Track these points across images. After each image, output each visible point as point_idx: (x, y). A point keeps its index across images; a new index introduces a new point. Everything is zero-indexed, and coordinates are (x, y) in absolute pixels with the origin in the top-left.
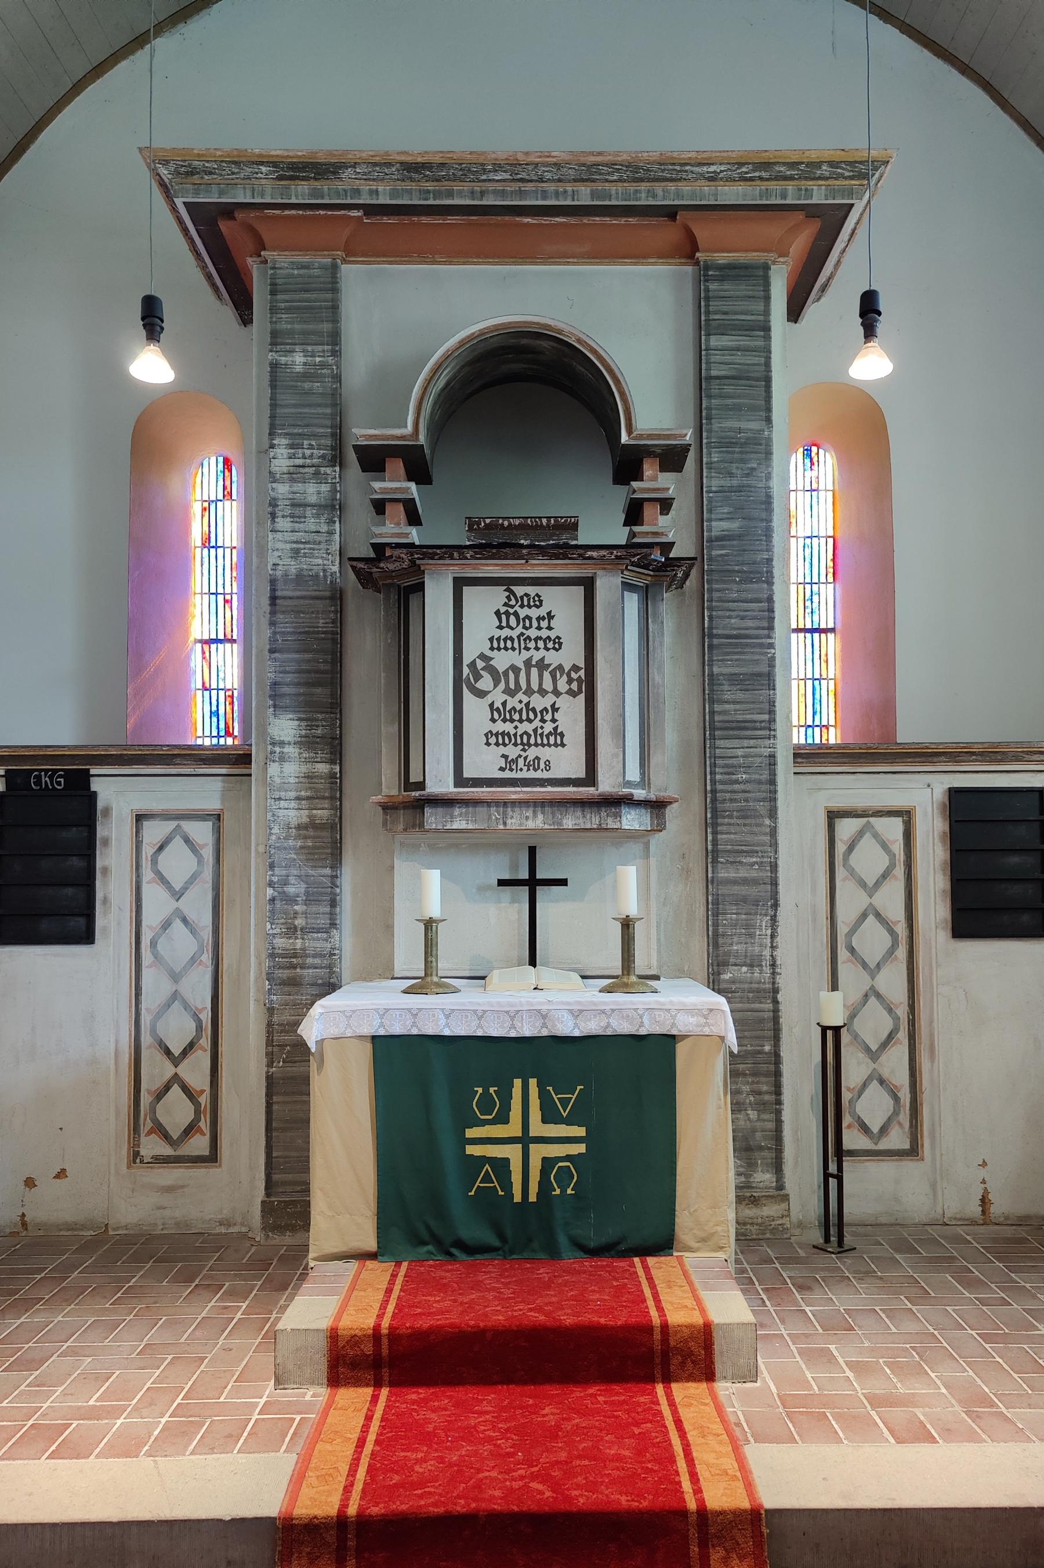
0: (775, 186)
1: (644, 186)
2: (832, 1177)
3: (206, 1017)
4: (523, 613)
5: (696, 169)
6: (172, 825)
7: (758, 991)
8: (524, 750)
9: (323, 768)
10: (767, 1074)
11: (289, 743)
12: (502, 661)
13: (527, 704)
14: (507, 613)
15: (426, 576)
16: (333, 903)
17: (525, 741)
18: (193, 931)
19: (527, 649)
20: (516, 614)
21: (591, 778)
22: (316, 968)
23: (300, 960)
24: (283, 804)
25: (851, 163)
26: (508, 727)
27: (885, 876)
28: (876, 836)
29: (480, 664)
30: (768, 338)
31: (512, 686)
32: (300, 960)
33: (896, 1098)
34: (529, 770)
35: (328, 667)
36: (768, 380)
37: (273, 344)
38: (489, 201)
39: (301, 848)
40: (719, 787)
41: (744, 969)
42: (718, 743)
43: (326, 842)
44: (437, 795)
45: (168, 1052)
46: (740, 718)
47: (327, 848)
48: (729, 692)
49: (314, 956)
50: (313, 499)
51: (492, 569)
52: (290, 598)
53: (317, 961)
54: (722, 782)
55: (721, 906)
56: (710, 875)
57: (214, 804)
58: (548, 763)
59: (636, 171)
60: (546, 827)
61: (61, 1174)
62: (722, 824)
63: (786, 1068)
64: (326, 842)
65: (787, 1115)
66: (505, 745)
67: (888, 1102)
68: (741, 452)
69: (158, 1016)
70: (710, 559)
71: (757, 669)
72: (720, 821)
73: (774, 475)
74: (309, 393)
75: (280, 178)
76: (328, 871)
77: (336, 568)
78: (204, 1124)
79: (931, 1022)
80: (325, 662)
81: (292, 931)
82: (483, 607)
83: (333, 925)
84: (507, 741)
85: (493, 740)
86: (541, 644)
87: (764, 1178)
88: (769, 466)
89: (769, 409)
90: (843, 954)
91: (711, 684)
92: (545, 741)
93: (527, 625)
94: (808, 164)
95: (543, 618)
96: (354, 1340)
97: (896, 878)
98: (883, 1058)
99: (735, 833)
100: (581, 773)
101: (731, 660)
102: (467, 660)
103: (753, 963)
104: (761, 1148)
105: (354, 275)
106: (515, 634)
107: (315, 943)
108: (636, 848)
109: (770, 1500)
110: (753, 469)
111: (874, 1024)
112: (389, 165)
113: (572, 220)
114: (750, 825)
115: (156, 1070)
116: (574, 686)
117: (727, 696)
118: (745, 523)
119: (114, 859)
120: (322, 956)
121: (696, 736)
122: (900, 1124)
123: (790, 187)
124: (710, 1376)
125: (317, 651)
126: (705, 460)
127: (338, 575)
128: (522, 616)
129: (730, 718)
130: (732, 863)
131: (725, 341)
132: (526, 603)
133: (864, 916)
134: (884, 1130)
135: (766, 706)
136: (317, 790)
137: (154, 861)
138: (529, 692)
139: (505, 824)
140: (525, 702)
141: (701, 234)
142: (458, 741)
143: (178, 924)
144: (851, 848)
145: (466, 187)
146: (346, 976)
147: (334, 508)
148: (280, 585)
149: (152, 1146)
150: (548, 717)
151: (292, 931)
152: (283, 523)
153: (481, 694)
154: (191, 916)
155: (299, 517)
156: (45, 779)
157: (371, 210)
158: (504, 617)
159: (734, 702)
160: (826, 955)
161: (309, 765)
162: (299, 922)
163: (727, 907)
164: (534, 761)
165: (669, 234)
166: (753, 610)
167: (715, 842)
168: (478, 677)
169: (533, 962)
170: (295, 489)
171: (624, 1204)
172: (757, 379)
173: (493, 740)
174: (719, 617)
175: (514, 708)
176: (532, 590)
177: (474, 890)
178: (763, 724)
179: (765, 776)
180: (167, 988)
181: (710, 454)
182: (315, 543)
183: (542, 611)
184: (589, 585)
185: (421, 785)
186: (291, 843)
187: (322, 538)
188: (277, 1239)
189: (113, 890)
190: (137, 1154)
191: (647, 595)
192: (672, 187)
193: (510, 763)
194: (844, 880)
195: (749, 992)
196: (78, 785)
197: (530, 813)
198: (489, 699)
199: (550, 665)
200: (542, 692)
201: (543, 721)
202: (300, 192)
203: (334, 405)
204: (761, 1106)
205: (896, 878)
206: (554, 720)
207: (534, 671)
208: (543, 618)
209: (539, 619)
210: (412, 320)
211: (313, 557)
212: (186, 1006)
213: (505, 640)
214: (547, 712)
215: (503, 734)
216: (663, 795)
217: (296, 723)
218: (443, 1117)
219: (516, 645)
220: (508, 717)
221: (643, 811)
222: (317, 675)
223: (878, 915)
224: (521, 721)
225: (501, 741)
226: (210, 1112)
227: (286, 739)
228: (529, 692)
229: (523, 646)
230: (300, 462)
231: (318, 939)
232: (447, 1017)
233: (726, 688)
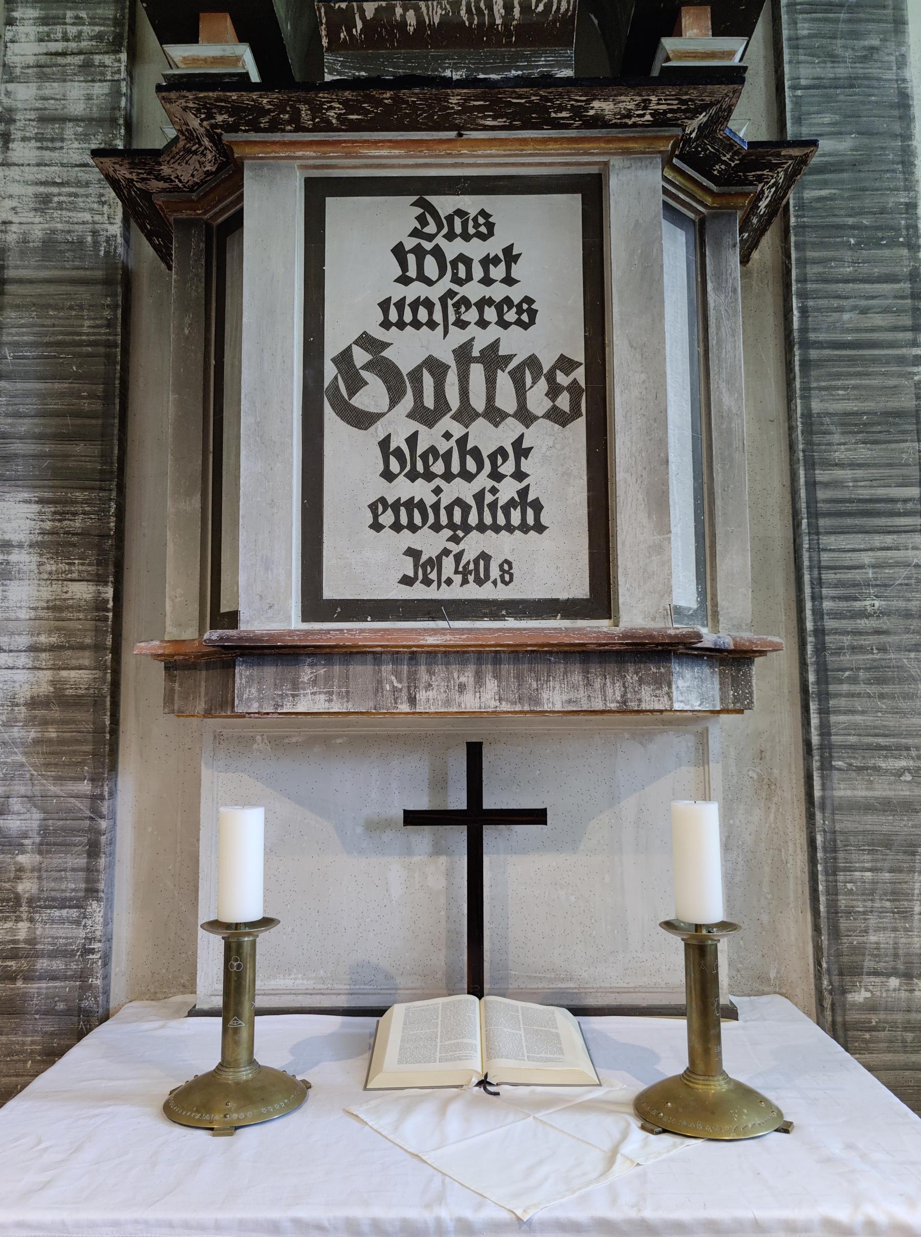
4: (451, 250)
8: (455, 539)
9: (82, 591)
11: (20, 546)
12: (407, 349)
13: (462, 441)
14: (419, 252)
15: (247, 174)
16: (93, 850)
17: (457, 518)
19: (462, 324)
20: (438, 253)
21: (601, 598)
22: (54, 978)
23: (24, 964)
26: (421, 490)
29: (361, 357)
31: (429, 402)
32: (24, 964)
34: (465, 582)
35: (98, 406)
39: (37, 742)
40: (830, 624)
41: (894, 982)
42: (825, 540)
44: (259, 638)
46: (865, 493)
47: (85, 742)
48: (842, 447)
49: (53, 955)
50: (77, 108)
51: (386, 155)
52: (31, 282)
53: (58, 965)
54: (837, 615)
55: (841, 855)
56: (817, 793)
58: (507, 568)
60: (505, 707)
62: (838, 695)
66: (413, 528)
68: (850, 21)
70: (801, 206)
71: (894, 404)
72: (832, 688)
76: (85, 787)
77: (116, 229)
80: (92, 396)
82: (367, 241)
83: (92, 892)
84: (418, 520)
85: (387, 518)
86: (490, 314)
88: (901, 43)
91: (809, 430)
92: (501, 521)
93: (462, 273)
95: (496, 261)
99: (863, 713)
100: (581, 589)
101: (845, 388)
102: (332, 348)
106: (434, 293)
107: (54, 929)
108: (680, 743)
110: (873, 49)
114: (892, 696)
116: (564, 402)
117: (840, 454)
118: (865, 140)
120: (66, 954)
125: (77, 377)
126: (785, 33)
127: (120, 240)
128: (450, 257)
129: (846, 494)
130: (860, 769)
132: (458, 229)
136: (69, 633)
138: (466, 415)
139: (412, 701)
140: (457, 435)
142: (301, 518)
146: (119, 988)
150: (507, 468)
153: (362, 420)
155: (52, 140)
158: (411, 259)
159: (853, 465)
161: (57, 587)
163: (854, 857)
164: (476, 562)
166: (885, 297)
168: (355, 384)
170: (48, 92)
173: (387, 518)
174: (818, 310)
175: (433, 450)
176: (471, 204)
177: (359, 830)
178: (909, 506)
181: (794, 23)
182: (78, 184)
183: (494, 247)
184: (592, 191)
185: (233, 619)
186: (17, 732)
191: (701, 235)
193: (425, 568)
195: (905, 1029)
198: (379, 430)
199: (510, 358)
200: (494, 415)
201: (496, 476)
206: (519, 475)
207: (477, 372)
208: (496, 261)
209: (486, 262)
211: (75, 209)
213: (415, 306)
214: (505, 457)
215: (410, 504)
216: (747, 637)
217: (36, 508)
219: (438, 316)
220: (420, 467)
221: (707, 671)
222: (79, 421)
224: (448, 476)
225: (404, 520)
227: (15, 538)
228: (466, 415)
229: (452, 318)
230: (59, 46)
231: (62, 921)
233: (836, 438)
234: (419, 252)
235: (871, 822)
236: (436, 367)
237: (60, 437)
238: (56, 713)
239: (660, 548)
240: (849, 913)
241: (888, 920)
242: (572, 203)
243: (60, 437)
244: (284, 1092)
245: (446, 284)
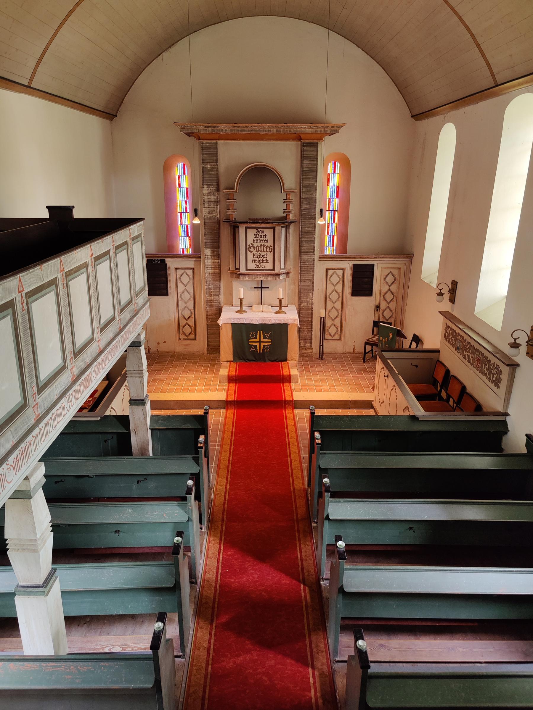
2: (321, 345)
3: (193, 311)
4: (260, 234)
9: (217, 261)
16: (219, 290)
21: (274, 269)
26: (257, 259)
28: (337, 274)
29: (251, 245)
33: (337, 329)
36: (317, 171)
43: (217, 276)
45: (185, 318)
50: (213, 200)
57: (192, 267)
61: (165, 342)
63: (313, 324)
64: (217, 276)
65: (313, 333)
69: (183, 311)
73: (317, 195)
78: (193, 333)
81: (211, 295)
82: (251, 233)
87: (308, 345)
89: (316, 179)
90: (328, 299)
96: (232, 376)
105: (220, 143)
107: (216, 298)
109: (295, 399)
111: (334, 314)
115: (183, 322)
121: (297, 253)
124: (290, 382)
133: (333, 291)
134: (334, 335)
137: (180, 278)
138: (261, 251)
142: (247, 261)
143: (186, 292)
144: (331, 277)
147: (217, 202)
149: (183, 337)
151: (211, 295)
152: (206, 206)
153: (251, 252)
154: (189, 290)
156: (156, 261)
160: (324, 300)
162: (212, 293)
167: (301, 277)
168: (250, 248)
169: (261, 304)
171: (277, 352)
179: (312, 263)
180: (184, 305)
183: (264, 234)
184: (274, 228)
185: (239, 269)
188: (210, 356)
189: (172, 284)
193: (257, 266)
196: (163, 261)
200: (264, 251)
203: (217, 177)
210: (235, 154)
212: (188, 309)
218: (245, 338)
223: (336, 291)
226: (194, 330)
228: (261, 251)
244: (245, 311)
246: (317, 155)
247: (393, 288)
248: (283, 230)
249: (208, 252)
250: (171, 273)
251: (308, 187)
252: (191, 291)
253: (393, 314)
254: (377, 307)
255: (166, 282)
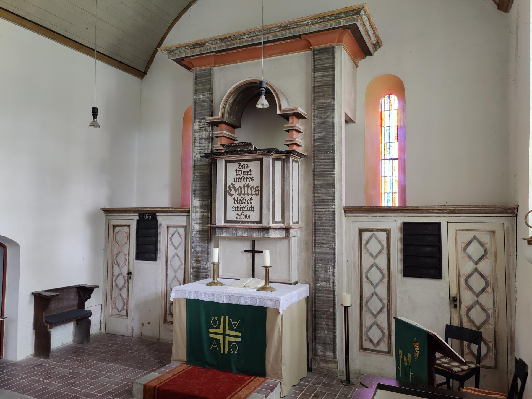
0: (329, 23)
1: (287, 31)
4: (243, 170)
5: (302, 23)
6: (175, 229)
7: (328, 291)
9: (206, 214)
10: (331, 319)
12: (237, 185)
16: (208, 254)
18: (180, 259)
20: (241, 171)
21: (261, 222)
24: (196, 225)
25: (351, 11)
26: (238, 205)
27: (380, 253)
28: (376, 238)
29: (231, 186)
30: (334, 71)
36: (334, 85)
37: (195, 93)
38: (244, 44)
41: (324, 283)
46: (323, 198)
50: (204, 137)
51: (233, 157)
53: (204, 270)
54: (318, 220)
59: (283, 28)
61: (149, 323)
67: (380, 333)
70: (314, 146)
71: (329, 182)
74: (203, 106)
75: (191, 49)
76: (206, 244)
79: (396, 307)
82: (233, 168)
83: (208, 260)
86: (248, 180)
87: (330, 354)
89: (334, 95)
90: (364, 279)
94: (336, 14)
97: (383, 253)
98: (378, 317)
103: (327, 281)
104: (329, 344)
106: (241, 177)
110: (329, 115)
111: (375, 305)
112: (216, 40)
113: (272, 44)
119: (162, 238)
120: (205, 269)
121: (311, 204)
122: (384, 342)
123: (333, 22)
131: (320, 74)
133: (372, 266)
134: (378, 343)
135: (332, 194)
137: (171, 239)
138: (244, 194)
141: (311, 40)
142: (225, 211)
143: (176, 257)
144: (368, 242)
145: (238, 41)
148: (196, 162)
150: (249, 202)
152: (197, 144)
153: (231, 195)
154: (179, 255)
157: (217, 52)
159: (322, 193)
160: (358, 279)
162: (199, 259)
165: (303, 43)
168: (231, 190)
169: (253, 276)
172: (330, 85)
173: (234, 209)
176: (245, 163)
179: (331, 218)
183: (248, 170)
184: (261, 160)
187: (206, 148)
189: (161, 247)
190: (166, 320)
192: (296, 30)
193: (239, 216)
194: (365, 253)
196: (154, 217)
197: (243, 232)
198: (234, 197)
200: (248, 194)
201: (248, 203)
202: (197, 51)
204: (329, 330)
205: (383, 253)
206: (251, 203)
207: (246, 188)
209: (247, 172)
210: (228, 79)
212: (178, 280)
223: (377, 266)
230: (201, 126)
232: (205, 295)
234: (239, 171)
235: (322, 256)
236: (240, 187)
237: (202, 190)
238: (203, 233)
239: (268, 214)
240: (318, 271)
241: (324, 272)
242: (259, 162)
243: (202, 190)
245: (242, 175)
246: (333, 62)
247: (485, 267)
248: (278, 164)
249: (197, 203)
250: (162, 230)
251: (321, 108)
252: (182, 256)
253: (488, 317)
254: (455, 302)
255: (155, 243)
